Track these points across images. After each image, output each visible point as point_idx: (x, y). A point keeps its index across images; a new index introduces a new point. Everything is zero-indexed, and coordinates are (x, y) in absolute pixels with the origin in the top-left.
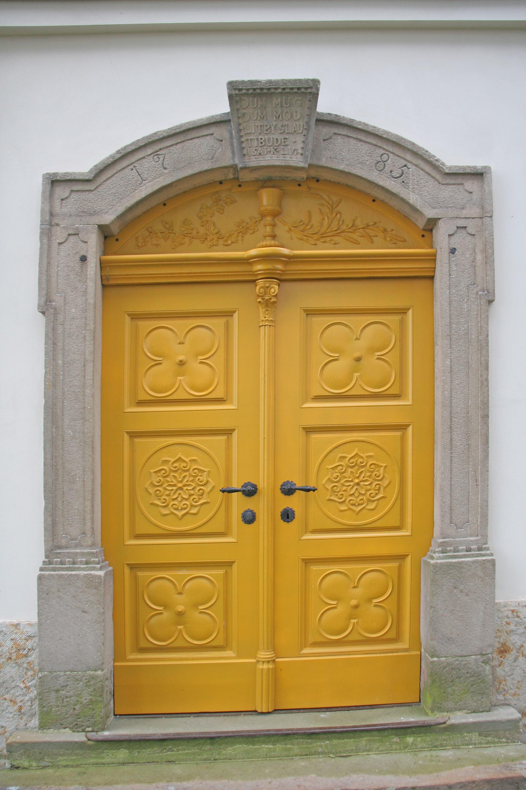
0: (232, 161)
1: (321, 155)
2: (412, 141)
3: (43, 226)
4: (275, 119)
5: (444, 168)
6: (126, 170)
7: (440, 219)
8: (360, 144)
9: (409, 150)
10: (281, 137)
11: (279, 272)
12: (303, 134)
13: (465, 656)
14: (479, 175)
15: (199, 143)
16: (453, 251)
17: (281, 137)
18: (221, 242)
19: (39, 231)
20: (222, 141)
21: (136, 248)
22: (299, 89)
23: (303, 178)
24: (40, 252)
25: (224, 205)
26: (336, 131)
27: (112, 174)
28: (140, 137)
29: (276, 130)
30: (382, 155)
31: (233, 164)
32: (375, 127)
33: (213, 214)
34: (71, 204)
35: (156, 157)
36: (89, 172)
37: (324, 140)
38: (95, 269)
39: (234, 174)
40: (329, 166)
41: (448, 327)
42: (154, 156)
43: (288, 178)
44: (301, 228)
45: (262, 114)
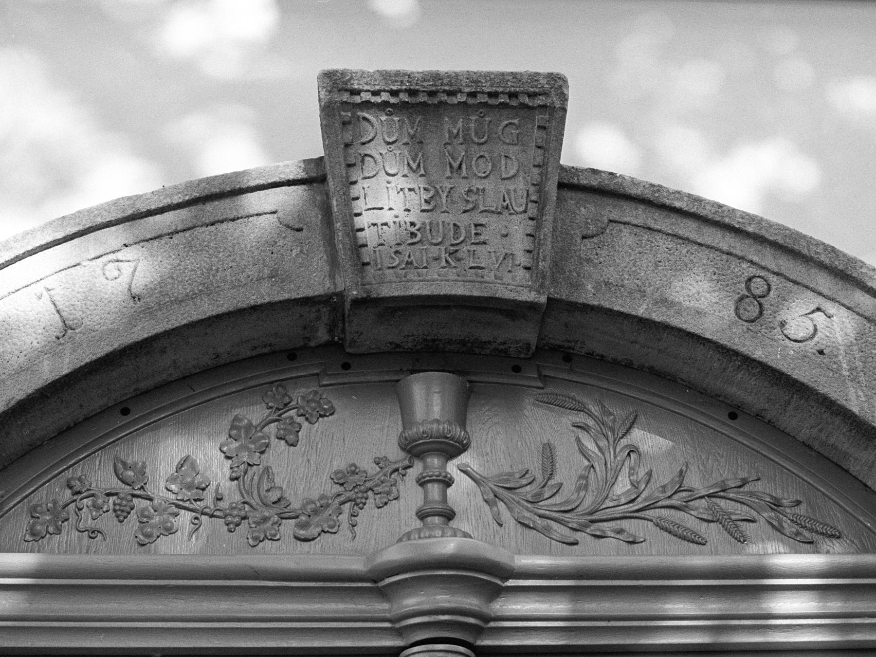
0: (328, 284)
2: (826, 242)
4: (448, 174)
9: (822, 266)
11: (472, 620)
12: (530, 213)
17: (465, 221)
18: (288, 527)
20: (300, 230)
21: (28, 537)
22: (513, 95)
23: (528, 345)
25: (299, 420)
26: (614, 216)
29: (453, 202)
30: (750, 280)
31: (332, 290)
33: (267, 445)
37: (584, 237)
39: (330, 331)
40: (607, 305)
43: (484, 344)
44: (529, 491)
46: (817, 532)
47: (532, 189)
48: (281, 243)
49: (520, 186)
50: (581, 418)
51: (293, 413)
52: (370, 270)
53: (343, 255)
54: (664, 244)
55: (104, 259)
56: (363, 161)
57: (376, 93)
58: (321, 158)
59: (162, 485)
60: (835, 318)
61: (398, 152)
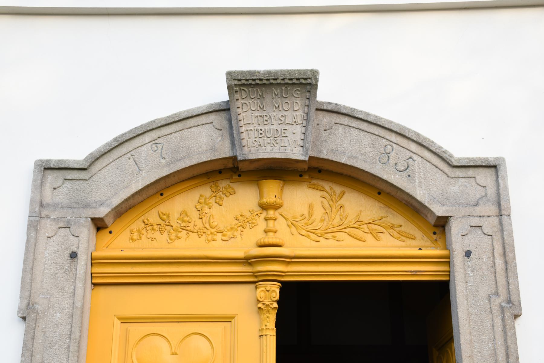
1: (321, 146)
3: (31, 218)
5: (453, 160)
6: (123, 159)
7: (451, 217)
8: (362, 134)
9: (413, 141)
10: (279, 128)
13: (34, 253)
14: (493, 167)
15: (198, 132)
16: (468, 254)
19: (26, 223)
24: (26, 247)
26: (338, 121)
27: (109, 162)
28: (138, 125)
32: (377, 117)
34: (60, 191)
35: (154, 146)
36: (85, 160)
37: (325, 130)
38: (85, 268)
41: (468, 345)
42: (152, 145)
45: (262, 104)
46: (406, 237)
47: (305, 115)
48: (214, 135)
49: (300, 113)
50: (324, 194)
51: (221, 193)
52: (246, 148)
53: (237, 143)
54: (354, 132)
55: (151, 143)
56: (243, 105)
57: (247, 80)
58: (228, 101)
59: (176, 221)
60: (416, 162)
61: (256, 102)
